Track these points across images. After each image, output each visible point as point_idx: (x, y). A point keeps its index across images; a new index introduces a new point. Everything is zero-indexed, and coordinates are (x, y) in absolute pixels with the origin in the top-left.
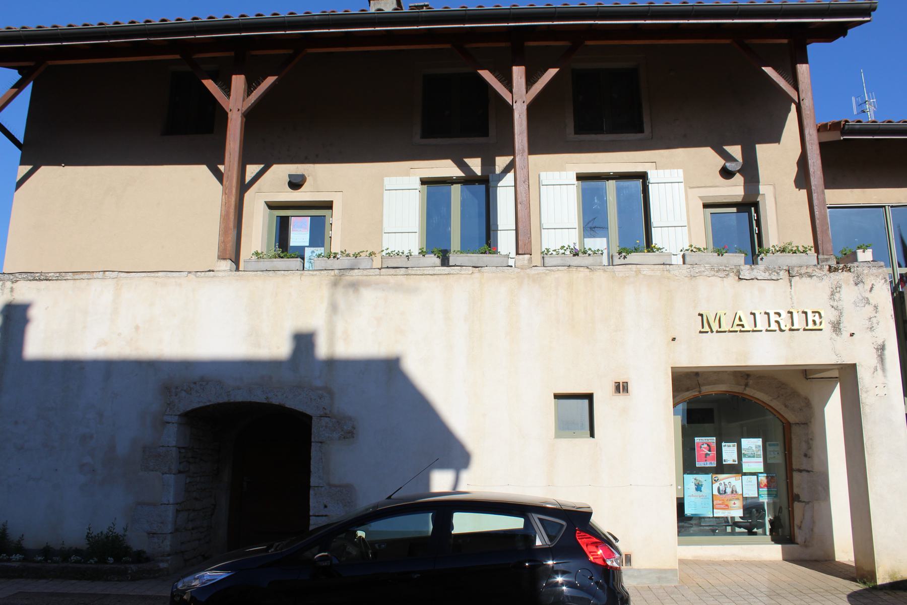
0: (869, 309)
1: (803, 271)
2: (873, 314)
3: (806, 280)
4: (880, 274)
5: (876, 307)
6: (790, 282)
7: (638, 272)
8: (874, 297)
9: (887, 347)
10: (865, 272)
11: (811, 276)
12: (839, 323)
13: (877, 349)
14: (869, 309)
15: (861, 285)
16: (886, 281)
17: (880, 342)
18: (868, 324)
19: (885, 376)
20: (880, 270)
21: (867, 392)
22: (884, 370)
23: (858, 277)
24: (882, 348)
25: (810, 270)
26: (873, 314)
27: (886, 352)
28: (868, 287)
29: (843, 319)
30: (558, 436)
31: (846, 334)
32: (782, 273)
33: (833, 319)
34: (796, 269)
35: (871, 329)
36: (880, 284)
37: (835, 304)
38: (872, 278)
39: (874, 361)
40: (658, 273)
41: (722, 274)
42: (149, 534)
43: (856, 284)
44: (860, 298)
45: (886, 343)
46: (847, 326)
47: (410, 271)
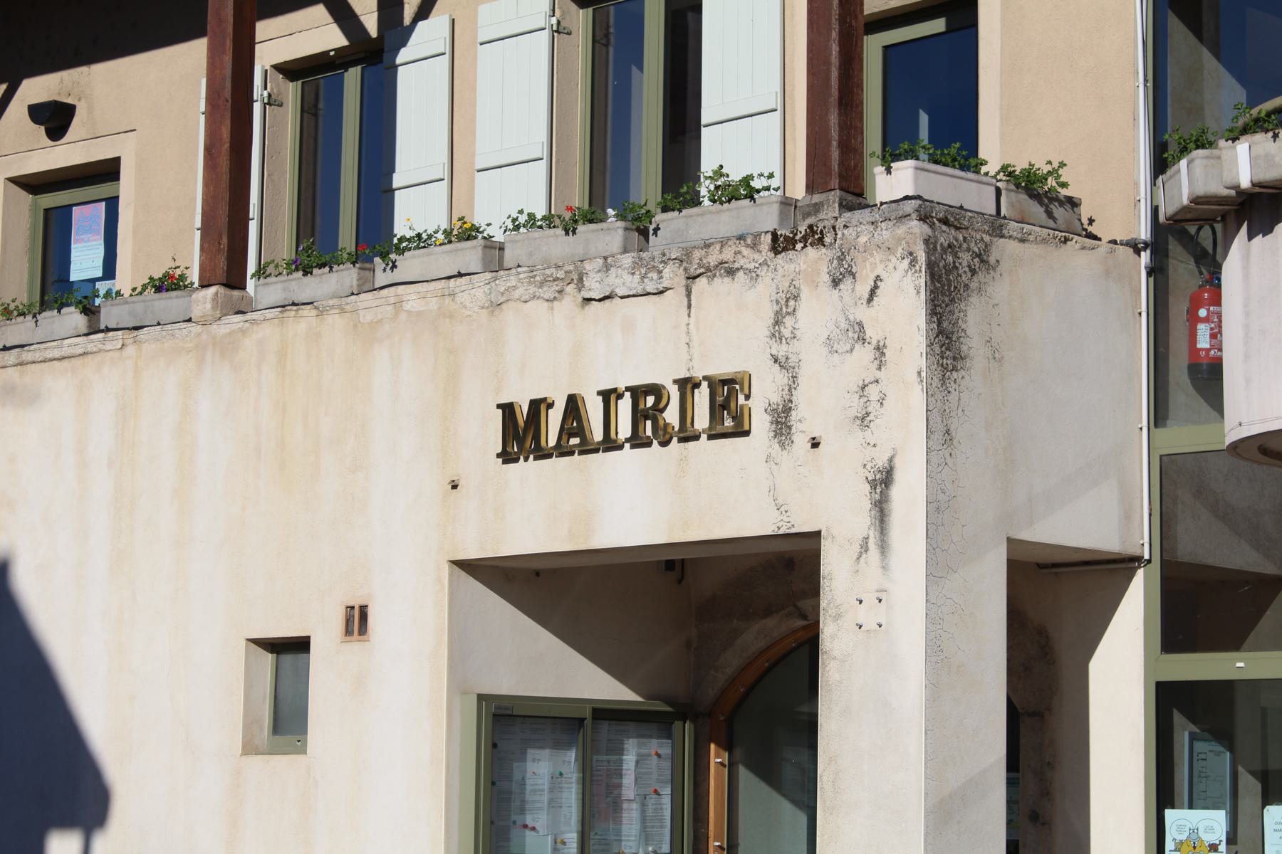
0: (865, 354)
1: (713, 260)
2: (873, 373)
3: (722, 284)
4: (899, 240)
5: (880, 350)
6: (689, 295)
7: (398, 304)
8: (877, 321)
9: (898, 476)
10: (863, 239)
11: (731, 272)
12: (787, 410)
13: (873, 484)
14: (865, 354)
15: (846, 285)
16: (913, 262)
17: (882, 462)
18: (856, 405)
19: (885, 568)
20: (901, 230)
21: (838, 617)
22: (884, 547)
23: (841, 260)
24: (883, 480)
25: (728, 254)
26: (873, 373)
27: (896, 492)
28: (863, 289)
29: (799, 396)
30: (309, 637)
31: (801, 441)
32: (667, 272)
33: (776, 398)
34: (697, 254)
35: (864, 420)
36: (900, 272)
37: (781, 350)
38: (878, 256)
39: (860, 520)
40: (434, 304)
41: (548, 292)
42: (644, 233)
43: (836, 283)
44: (844, 325)
45: (898, 463)
46: (805, 422)
47: (26, 355)
